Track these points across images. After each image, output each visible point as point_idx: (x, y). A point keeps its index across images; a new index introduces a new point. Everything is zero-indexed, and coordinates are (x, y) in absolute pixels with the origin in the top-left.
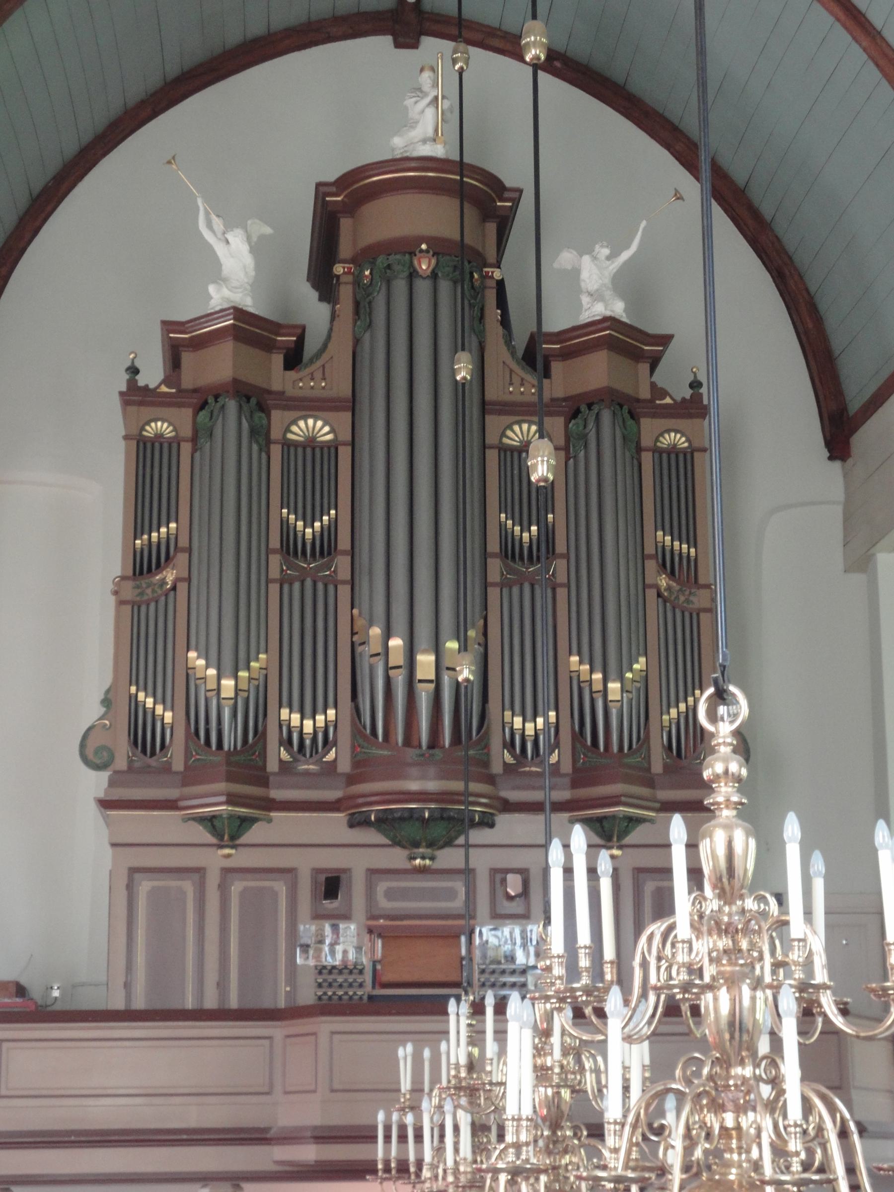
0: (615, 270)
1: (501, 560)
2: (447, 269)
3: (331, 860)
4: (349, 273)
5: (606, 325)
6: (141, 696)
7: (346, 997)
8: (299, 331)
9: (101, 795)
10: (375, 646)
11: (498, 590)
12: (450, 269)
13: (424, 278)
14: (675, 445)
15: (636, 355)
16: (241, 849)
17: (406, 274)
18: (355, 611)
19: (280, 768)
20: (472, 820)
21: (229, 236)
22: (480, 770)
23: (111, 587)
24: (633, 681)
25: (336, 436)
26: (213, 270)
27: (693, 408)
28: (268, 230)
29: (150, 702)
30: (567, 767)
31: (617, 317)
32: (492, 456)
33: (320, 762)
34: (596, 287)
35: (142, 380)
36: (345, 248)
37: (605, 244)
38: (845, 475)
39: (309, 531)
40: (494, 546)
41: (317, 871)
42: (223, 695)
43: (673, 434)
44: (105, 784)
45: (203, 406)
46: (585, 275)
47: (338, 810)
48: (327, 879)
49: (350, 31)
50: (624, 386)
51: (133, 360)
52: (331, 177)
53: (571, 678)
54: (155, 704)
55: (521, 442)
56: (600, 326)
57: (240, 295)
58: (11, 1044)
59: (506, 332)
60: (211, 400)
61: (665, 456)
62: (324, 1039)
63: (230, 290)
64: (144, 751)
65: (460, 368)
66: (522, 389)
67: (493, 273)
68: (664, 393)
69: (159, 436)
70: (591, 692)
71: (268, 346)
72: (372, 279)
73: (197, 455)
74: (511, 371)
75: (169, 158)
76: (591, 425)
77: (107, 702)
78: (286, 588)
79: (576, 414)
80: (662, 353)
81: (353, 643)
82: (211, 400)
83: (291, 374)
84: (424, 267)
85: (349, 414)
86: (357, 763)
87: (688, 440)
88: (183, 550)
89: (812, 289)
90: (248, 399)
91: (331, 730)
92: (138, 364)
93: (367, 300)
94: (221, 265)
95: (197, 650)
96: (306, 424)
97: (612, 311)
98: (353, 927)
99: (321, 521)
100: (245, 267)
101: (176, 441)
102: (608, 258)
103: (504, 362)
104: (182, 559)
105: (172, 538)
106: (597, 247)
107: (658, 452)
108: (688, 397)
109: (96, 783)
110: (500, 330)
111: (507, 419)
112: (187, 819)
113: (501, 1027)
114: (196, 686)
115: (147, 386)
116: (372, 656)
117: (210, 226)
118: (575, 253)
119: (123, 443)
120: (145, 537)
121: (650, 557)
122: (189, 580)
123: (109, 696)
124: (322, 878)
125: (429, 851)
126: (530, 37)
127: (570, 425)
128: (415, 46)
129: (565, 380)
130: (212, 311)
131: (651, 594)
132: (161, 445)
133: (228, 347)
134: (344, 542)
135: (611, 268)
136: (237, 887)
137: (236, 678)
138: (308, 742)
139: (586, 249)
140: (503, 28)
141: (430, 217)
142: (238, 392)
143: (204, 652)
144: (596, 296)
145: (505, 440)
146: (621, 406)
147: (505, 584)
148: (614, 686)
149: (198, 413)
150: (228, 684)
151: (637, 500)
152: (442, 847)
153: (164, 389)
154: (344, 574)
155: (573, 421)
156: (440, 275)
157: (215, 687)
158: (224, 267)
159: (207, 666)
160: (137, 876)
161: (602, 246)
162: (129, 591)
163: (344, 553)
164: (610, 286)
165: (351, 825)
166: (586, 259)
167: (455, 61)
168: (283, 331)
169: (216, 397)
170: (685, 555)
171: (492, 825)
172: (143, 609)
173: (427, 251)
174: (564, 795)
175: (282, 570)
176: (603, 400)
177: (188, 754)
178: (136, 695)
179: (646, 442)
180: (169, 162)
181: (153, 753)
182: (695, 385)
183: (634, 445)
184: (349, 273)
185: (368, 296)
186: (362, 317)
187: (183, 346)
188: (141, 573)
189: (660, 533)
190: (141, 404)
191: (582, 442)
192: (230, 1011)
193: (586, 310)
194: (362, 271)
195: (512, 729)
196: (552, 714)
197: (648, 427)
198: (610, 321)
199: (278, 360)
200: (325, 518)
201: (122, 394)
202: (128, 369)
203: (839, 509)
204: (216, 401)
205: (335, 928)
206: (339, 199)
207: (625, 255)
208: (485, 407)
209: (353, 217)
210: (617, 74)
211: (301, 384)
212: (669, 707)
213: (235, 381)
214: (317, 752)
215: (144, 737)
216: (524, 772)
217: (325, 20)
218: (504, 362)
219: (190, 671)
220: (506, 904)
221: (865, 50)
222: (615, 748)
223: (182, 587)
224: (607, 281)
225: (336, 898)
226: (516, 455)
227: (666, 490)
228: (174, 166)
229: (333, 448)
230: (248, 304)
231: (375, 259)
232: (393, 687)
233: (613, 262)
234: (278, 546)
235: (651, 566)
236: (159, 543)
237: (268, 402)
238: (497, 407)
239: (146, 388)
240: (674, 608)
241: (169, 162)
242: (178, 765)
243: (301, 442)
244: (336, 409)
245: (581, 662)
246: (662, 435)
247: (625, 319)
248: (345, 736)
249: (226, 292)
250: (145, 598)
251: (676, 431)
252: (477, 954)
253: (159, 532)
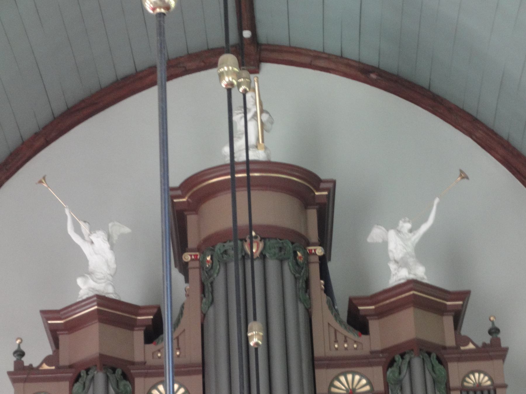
0: (417, 240)
2: (273, 251)
4: (196, 259)
8: (155, 310)
12: (277, 250)
15: (440, 310)
21: (93, 238)
26: (81, 266)
28: (127, 230)
31: (419, 279)
35: (27, 361)
36: (193, 241)
37: (407, 219)
46: (391, 246)
49: (203, 64)
50: (431, 336)
51: (19, 345)
56: (405, 288)
57: (103, 285)
59: (329, 298)
63: (96, 282)
65: (252, 336)
66: (346, 345)
67: (315, 250)
68: (467, 340)
71: (130, 325)
72: (212, 264)
74: (336, 331)
75: (40, 178)
79: (391, 363)
80: (464, 307)
82: (83, 373)
83: (151, 347)
85: (200, 377)
87: (490, 379)
90: (114, 370)
92: (23, 348)
93: (210, 281)
94: (87, 261)
97: (415, 275)
100: (107, 261)
102: (411, 231)
103: (329, 324)
106: (401, 222)
108: (488, 342)
115: (31, 365)
118: (383, 228)
126: (223, 67)
127: (388, 373)
129: (383, 334)
130: (80, 300)
133: (94, 329)
135: (413, 239)
139: (393, 225)
140: (327, 51)
141: (271, 210)
142: (104, 365)
144: (402, 263)
146: (429, 354)
149: (73, 385)
153: (45, 367)
155: (390, 370)
156: (267, 255)
158: (90, 263)
161: (405, 222)
164: (413, 254)
168: (141, 311)
169: (87, 371)
176: (412, 350)
180: (41, 182)
182: (494, 331)
183: (443, 386)
184: (196, 259)
185: (210, 277)
186: (207, 294)
190: (25, 381)
191: (398, 387)
193: (394, 275)
194: (204, 258)
199: (139, 335)
201: (9, 373)
202: (15, 353)
204: (87, 374)
206: (184, 200)
207: (424, 228)
208: (314, 363)
209: (197, 214)
210: (422, 80)
211: (159, 355)
213: (102, 356)
217: (181, 57)
218: (329, 324)
224: (410, 249)
228: (45, 185)
230: (110, 292)
231: (214, 246)
233: (414, 234)
237: (132, 371)
238: (325, 362)
241: (41, 182)
247: (426, 281)
249: (92, 283)
251: (480, 372)
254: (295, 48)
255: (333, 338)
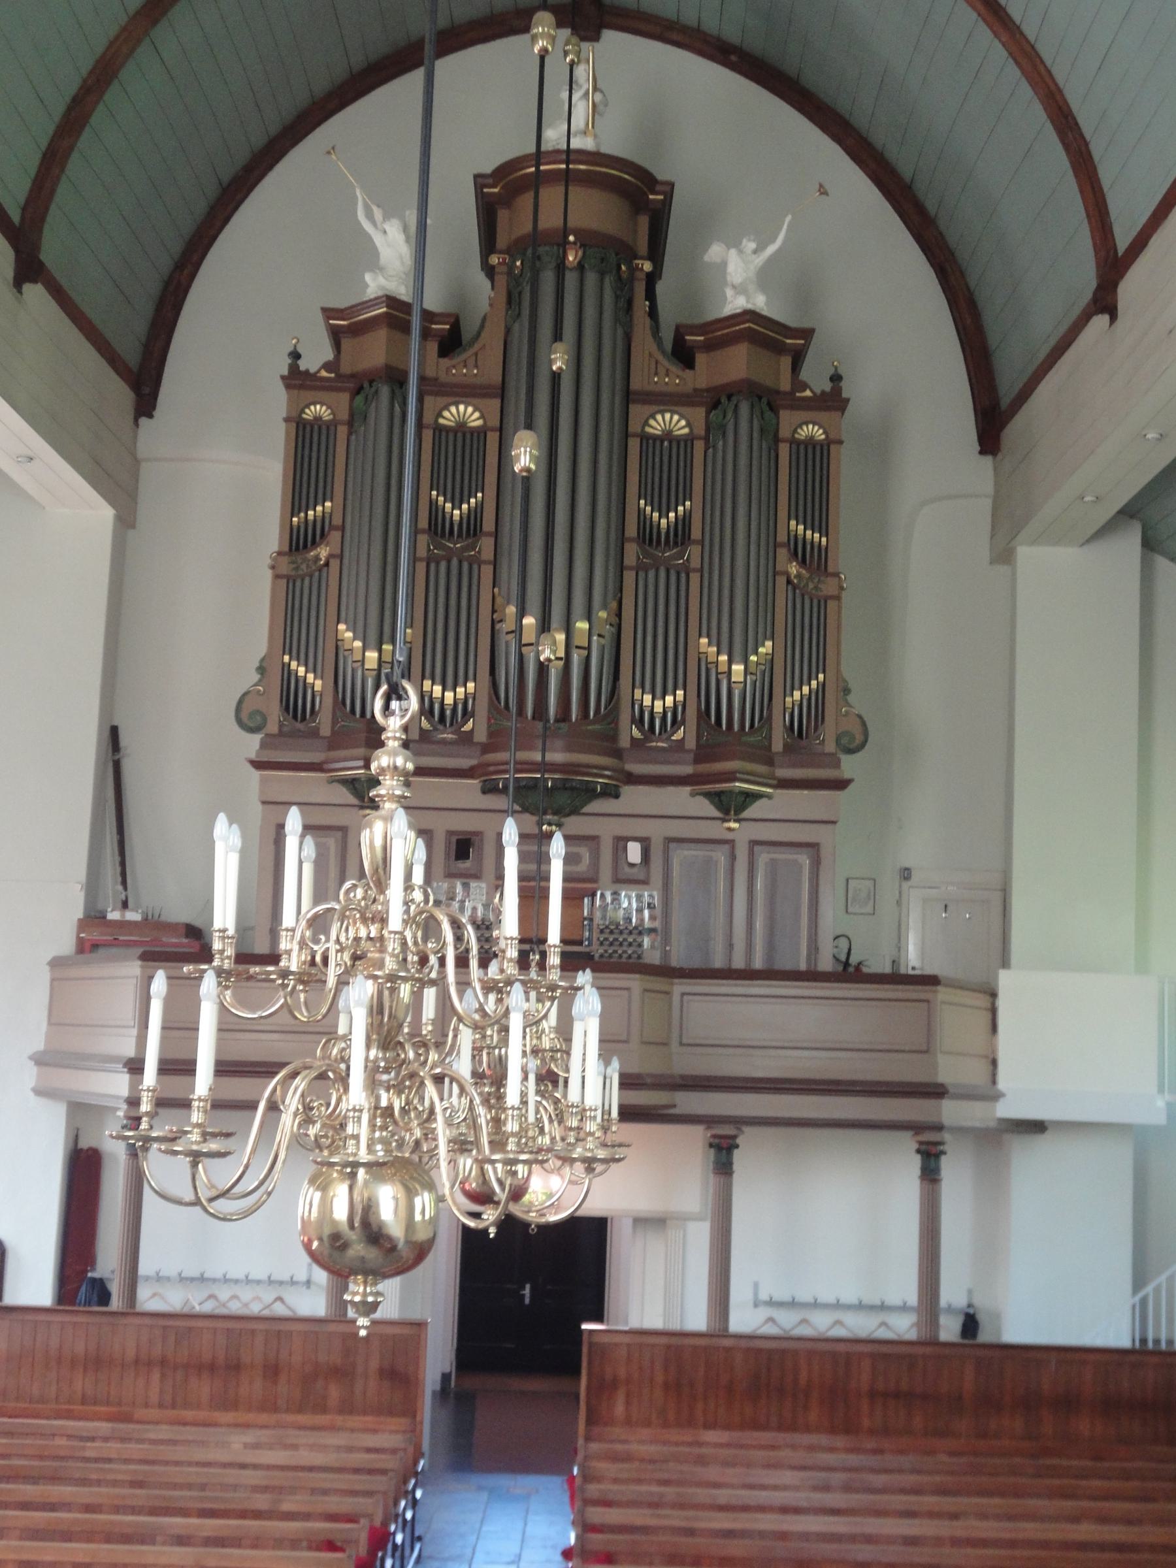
1: (638, 544)
3: (465, 824)
5: (748, 317)
6: (294, 664)
7: (625, 956)
8: (452, 320)
9: (253, 756)
10: (509, 625)
11: (634, 573)
13: (571, 270)
14: (812, 437)
15: (778, 348)
16: (743, 823)
17: (553, 265)
18: (496, 590)
19: (420, 735)
20: (595, 790)
21: (387, 227)
22: (608, 742)
23: (269, 561)
24: (758, 664)
25: (485, 422)
26: (370, 258)
27: (833, 401)
29: (302, 671)
30: (691, 744)
32: (634, 445)
33: (457, 732)
34: (740, 280)
35: (303, 365)
38: (995, 469)
39: (456, 512)
40: (631, 530)
41: (450, 833)
42: (366, 667)
43: (312, 408)
44: (257, 746)
45: (359, 390)
46: (731, 268)
47: (472, 777)
48: (458, 841)
52: (488, 169)
53: (699, 660)
54: (306, 672)
55: (663, 431)
58: (690, 997)
60: (366, 385)
61: (802, 447)
62: (676, 998)
64: (295, 717)
68: (804, 386)
69: (318, 419)
70: (717, 673)
73: (353, 437)
75: (329, 148)
76: (730, 415)
77: (261, 670)
78: (433, 566)
81: (493, 620)
82: (366, 385)
83: (445, 362)
84: (571, 258)
86: (491, 734)
87: (825, 432)
88: (336, 528)
89: (972, 284)
91: (470, 702)
92: (300, 350)
95: (346, 623)
96: (671, 418)
98: (484, 885)
99: (469, 503)
100: (401, 257)
101: (331, 426)
102: (755, 252)
104: (335, 536)
105: (327, 516)
106: (744, 241)
107: (795, 443)
109: (252, 744)
110: (648, 321)
111: (648, 409)
112: (332, 781)
113: (463, 979)
114: (345, 657)
116: (508, 633)
117: (370, 216)
119: (283, 425)
120: (302, 515)
121: (782, 545)
122: (341, 557)
123: (264, 664)
124: (454, 839)
125: (556, 818)
128: (596, 38)
129: (709, 371)
131: (781, 581)
132: (320, 428)
134: (488, 524)
136: (764, 857)
137: (380, 651)
138: (448, 712)
139: (736, 244)
141: (592, 211)
143: (351, 624)
144: (740, 290)
145: (648, 429)
147: (640, 568)
148: (738, 668)
150: (372, 655)
151: (772, 488)
152: (569, 815)
153: (324, 374)
154: (487, 552)
157: (360, 658)
159: (355, 639)
160: (757, 848)
161: (749, 240)
162: (285, 567)
163: (488, 534)
165: (484, 792)
166: (733, 252)
167: (566, 53)
169: (371, 382)
170: (816, 544)
171: (617, 796)
172: (298, 584)
173: (575, 243)
174: (687, 769)
175: (429, 550)
177: (334, 722)
178: (289, 665)
179: (784, 432)
180: (329, 153)
181: (304, 718)
182: (836, 378)
187: (344, 333)
188: (297, 549)
189: (793, 523)
190: (301, 387)
192: (736, 971)
194: (515, 262)
195: (641, 705)
196: (680, 693)
197: (787, 419)
198: (750, 315)
200: (473, 500)
201: (283, 377)
203: (986, 504)
204: (371, 386)
205: (466, 886)
206: (496, 190)
207: (771, 249)
212: (793, 689)
214: (666, 731)
215: (295, 704)
216: (657, 747)
219: (340, 643)
220: (627, 869)
221: (1004, 45)
222: (736, 727)
223: (335, 564)
225: (468, 858)
226: (658, 443)
227: (322, 466)
228: (333, 157)
229: (481, 432)
232: (525, 666)
234: (426, 526)
235: (783, 554)
236: (315, 521)
239: (307, 372)
240: (803, 596)
241: (329, 153)
242: (326, 731)
243: (450, 427)
244: (692, 404)
245: (710, 644)
246: (800, 426)
247: (765, 312)
248: (482, 709)
249: (382, 281)
250: (301, 572)
252: (598, 915)
253: (315, 510)
254: (644, 13)
255: (653, 371)
